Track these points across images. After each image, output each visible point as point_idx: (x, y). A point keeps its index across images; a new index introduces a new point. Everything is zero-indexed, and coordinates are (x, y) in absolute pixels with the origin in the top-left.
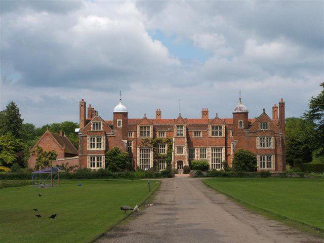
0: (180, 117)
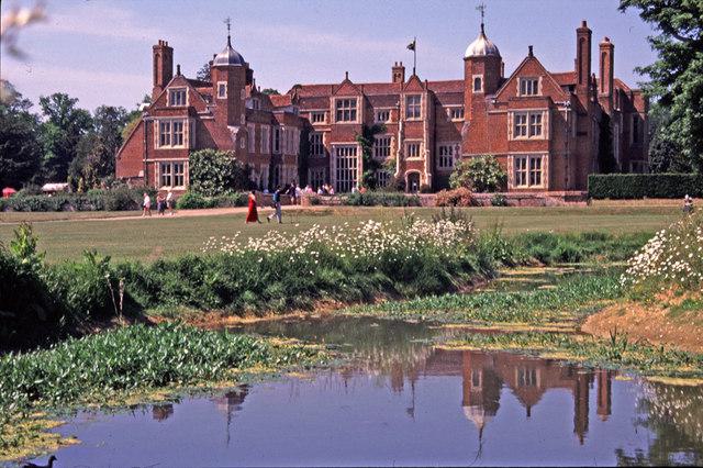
0: (347, 81)
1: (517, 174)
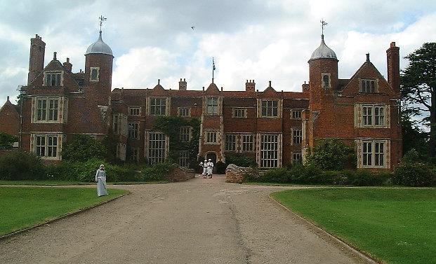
1: (365, 155)
